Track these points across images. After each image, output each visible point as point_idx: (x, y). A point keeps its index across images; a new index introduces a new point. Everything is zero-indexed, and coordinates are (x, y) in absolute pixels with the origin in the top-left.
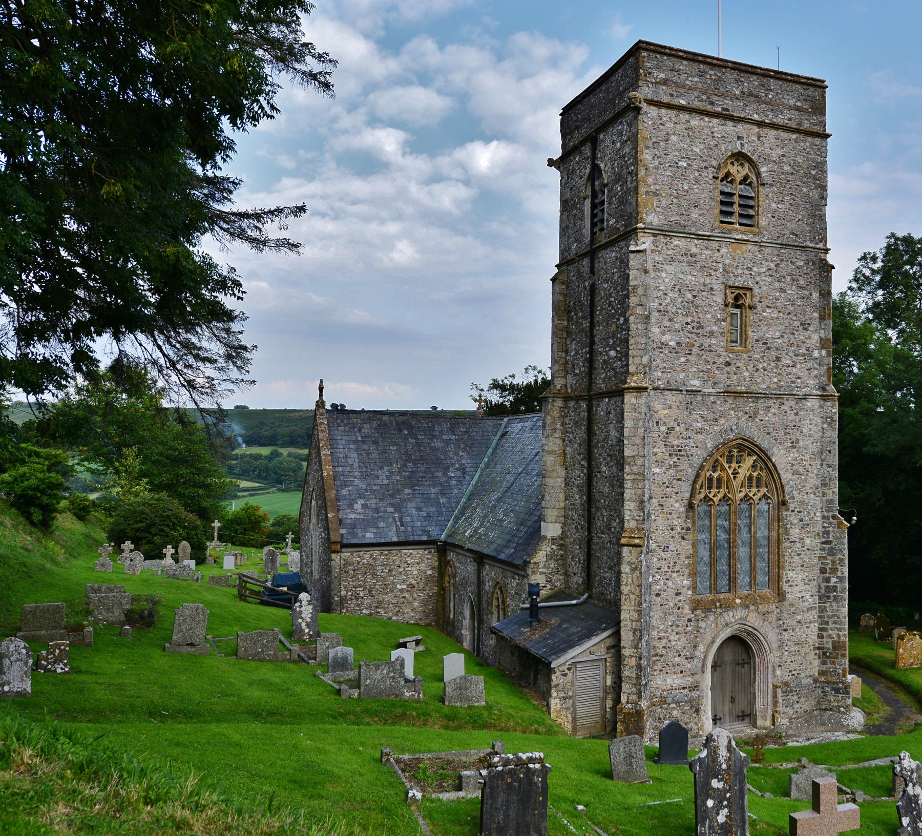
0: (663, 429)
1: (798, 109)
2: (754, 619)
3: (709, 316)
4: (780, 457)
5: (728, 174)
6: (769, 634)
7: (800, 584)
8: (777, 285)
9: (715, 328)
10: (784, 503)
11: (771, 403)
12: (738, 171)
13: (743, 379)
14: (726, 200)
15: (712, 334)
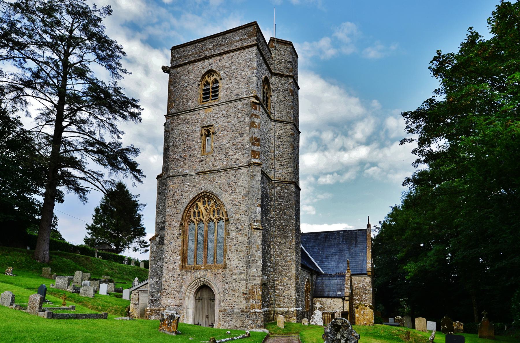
0: (172, 193)
1: (241, 40)
2: (209, 277)
3: (194, 142)
4: (226, 198)
5: (207, 82)
6: (217, 287)
7: (235, 260)
8: (227, 120)
9: (196, 147)
10: (227, 220)
11: (222, 174)
12: (210, 79)
13: (209, 165)
14: (206, 93)
15: (195, 149)
